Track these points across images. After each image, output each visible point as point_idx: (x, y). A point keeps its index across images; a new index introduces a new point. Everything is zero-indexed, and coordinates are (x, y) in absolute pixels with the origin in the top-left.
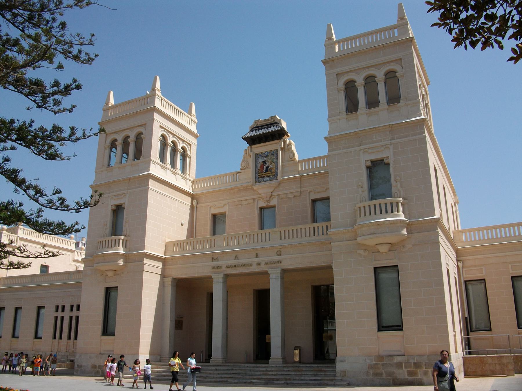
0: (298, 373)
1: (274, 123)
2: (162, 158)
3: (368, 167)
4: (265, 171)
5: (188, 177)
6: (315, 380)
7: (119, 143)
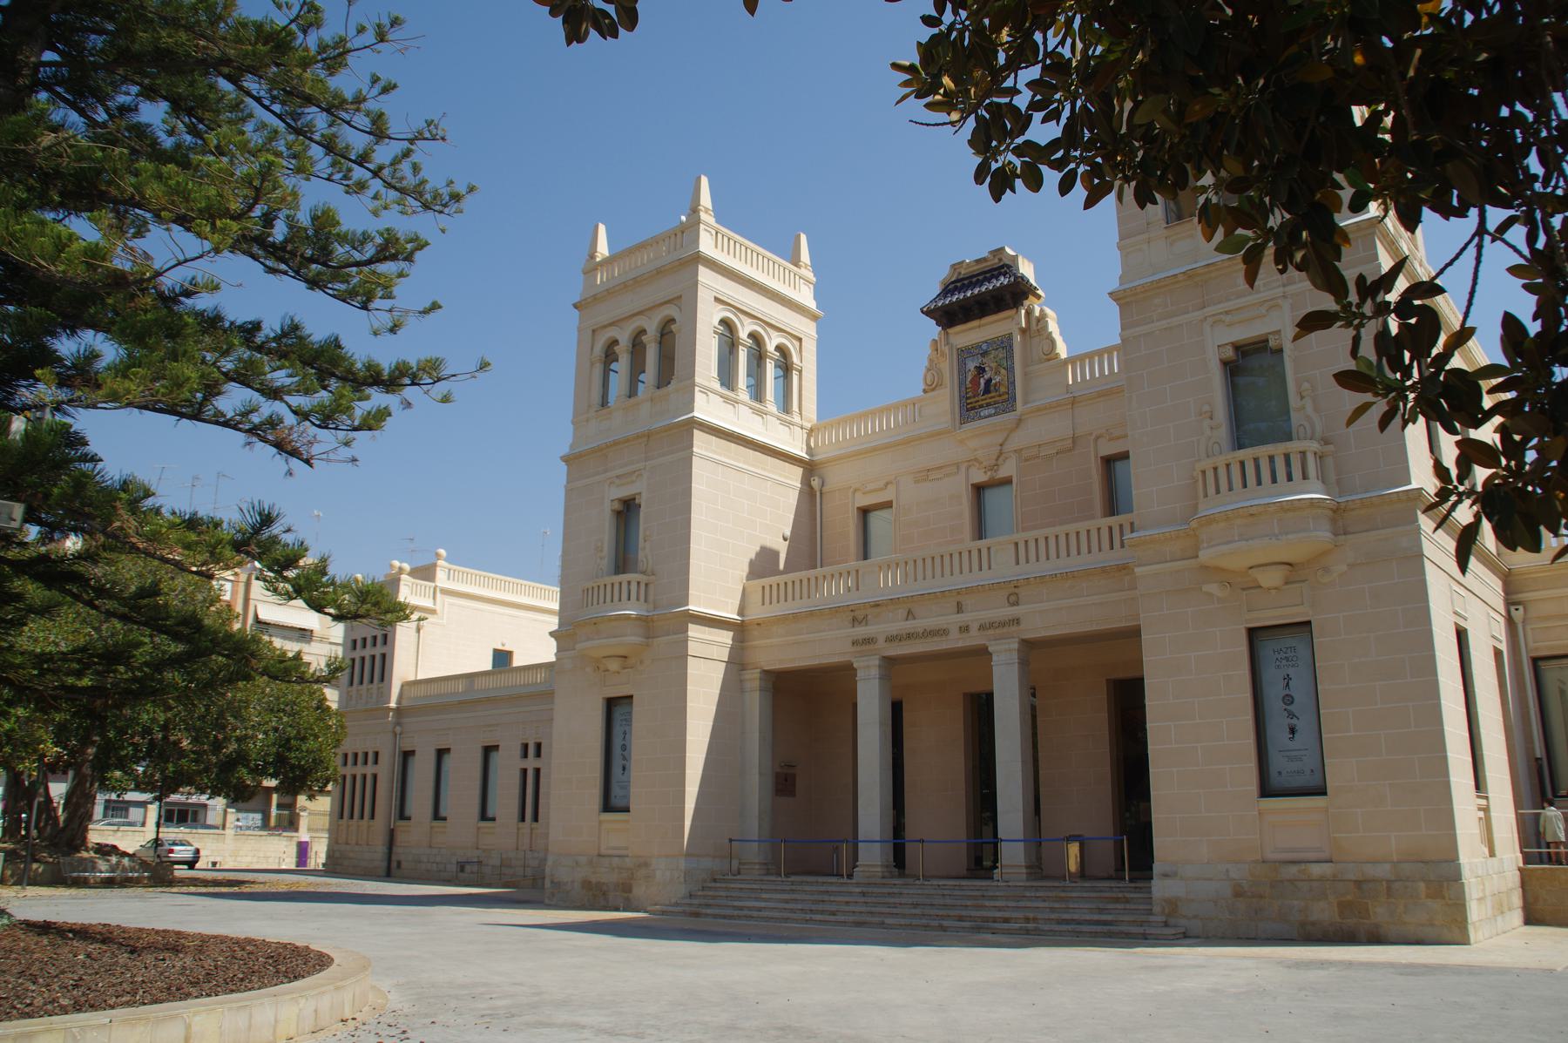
0: (1057, 905)
1: (1001, 267)
2: (727, 376)
3: (1225, 363)
4: (982, 390)
5: (797, 419)
6: (1098, 923)
7: (623, 351)
